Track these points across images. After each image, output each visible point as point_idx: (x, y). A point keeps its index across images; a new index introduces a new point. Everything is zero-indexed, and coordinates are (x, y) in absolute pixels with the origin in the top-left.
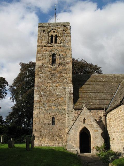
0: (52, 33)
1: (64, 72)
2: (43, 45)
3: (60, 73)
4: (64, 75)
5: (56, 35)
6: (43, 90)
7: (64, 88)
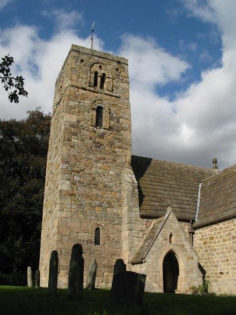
0: (96, 68)
1: (117, 144)
3: (111, 144)
4: (117, 150)
6: (79, 172)
7: (118, 175)
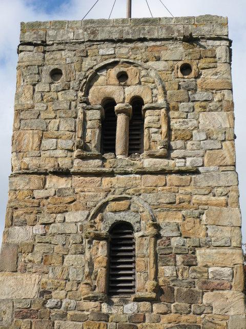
2: (49, 166)
5: (137, 102)
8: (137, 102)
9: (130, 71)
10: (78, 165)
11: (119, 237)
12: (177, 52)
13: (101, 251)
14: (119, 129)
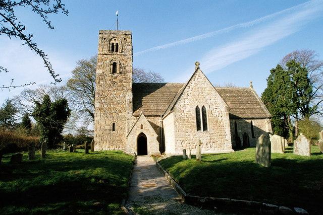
5: (117, 44)
8: (117, 44)
9: (116, 39)
10: (108, 53)
11: (114, 65)
12: (123, 36)
13: (112, 67)
14: (114, 48)
